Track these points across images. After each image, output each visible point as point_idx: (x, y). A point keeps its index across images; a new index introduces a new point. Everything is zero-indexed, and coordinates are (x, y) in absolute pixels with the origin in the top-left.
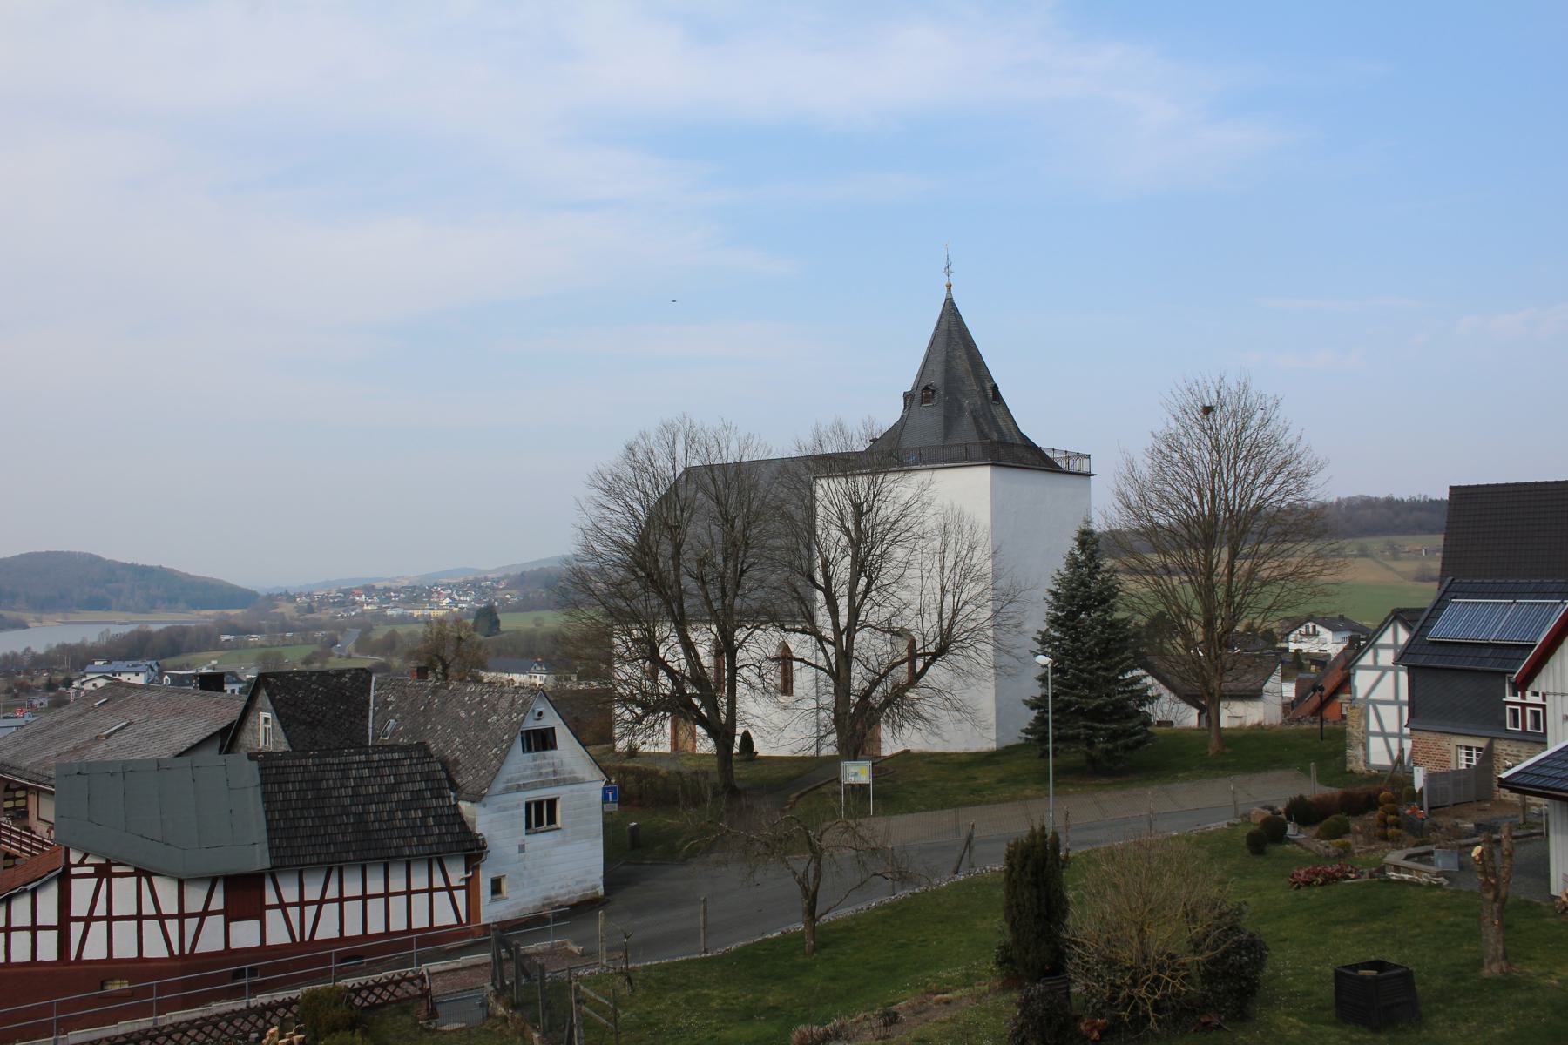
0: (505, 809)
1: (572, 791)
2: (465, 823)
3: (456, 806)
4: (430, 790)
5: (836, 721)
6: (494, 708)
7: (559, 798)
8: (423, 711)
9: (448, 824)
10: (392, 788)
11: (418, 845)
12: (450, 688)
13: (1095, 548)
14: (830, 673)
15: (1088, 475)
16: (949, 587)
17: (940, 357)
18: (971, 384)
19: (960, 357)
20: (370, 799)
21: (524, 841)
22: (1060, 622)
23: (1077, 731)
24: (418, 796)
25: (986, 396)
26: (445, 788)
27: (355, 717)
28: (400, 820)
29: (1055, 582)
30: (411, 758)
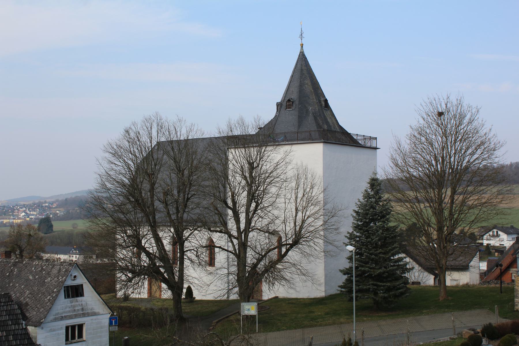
0: (54, 330)
1: (92, 320)
2: (31, 338)
3: (26, 329)
4: (11, 320)
5: (238, 281)
6: (49, 274)
7: (84, 323)
8: (8, 276)
12: (24, 263)
15: (376, 148)
16: (300, 208)
17: (296, 84)
18: (313, 99)
19: (307, 84)
23: (368, 287)
25: (321, 105)
26: (20, 319)
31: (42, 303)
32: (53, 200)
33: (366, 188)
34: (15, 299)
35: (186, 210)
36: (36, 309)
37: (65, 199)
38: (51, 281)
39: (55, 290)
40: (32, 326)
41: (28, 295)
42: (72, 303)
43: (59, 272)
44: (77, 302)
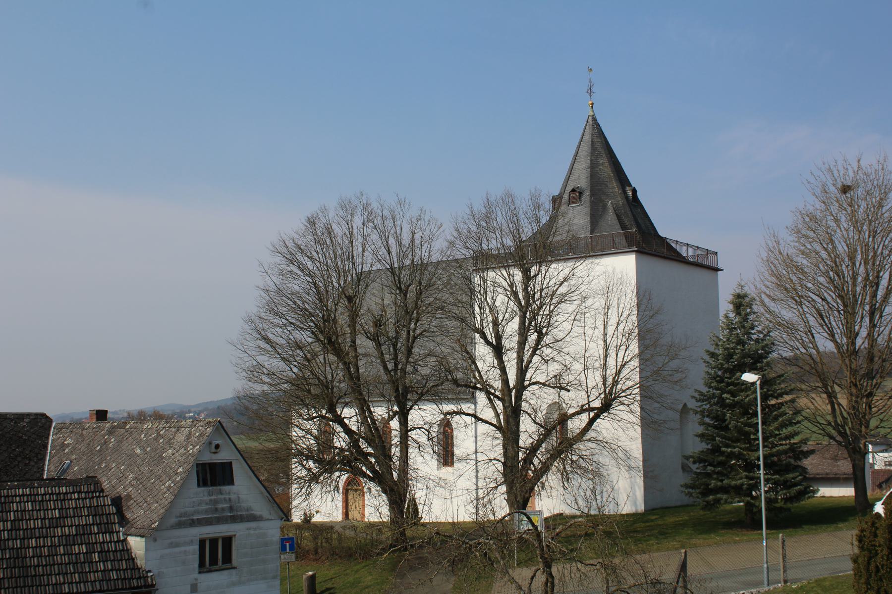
0: (177, 545)
1: (249, 529)
2: (133, 559)
3: (125, 540)
4: (97, 525)
5: (504, 475)
6: (170, 442)
7: (235, 535)
8: (100, 451)
9: (114, 560)
10: (56, 523)
11: (80, 582)
12: (127, 427)
13: (749, 310)
14: (499, 428)
15: (717, 270)
16: (613, 343)
19: (602, 164)
20: (30, 534)
21: (196, 579)
22: (718, 379)
24: (83, 532)
26: (115, 523)
27: (30, 460)
28: (61, 555)
29: (713, 342)
30: (80, 492)
31: (156, 493)
32: (200, 409)
33: (725, 312)
34: (108, 490)
35: (411, 360)
36: (145, 504)
37: (216, 407)
38: (173, 454)
39: (181, 470)
40: (136, 535)
41: (132, 481)
42: (212, 495)
43: (188, 439)
44: (221, 494)
